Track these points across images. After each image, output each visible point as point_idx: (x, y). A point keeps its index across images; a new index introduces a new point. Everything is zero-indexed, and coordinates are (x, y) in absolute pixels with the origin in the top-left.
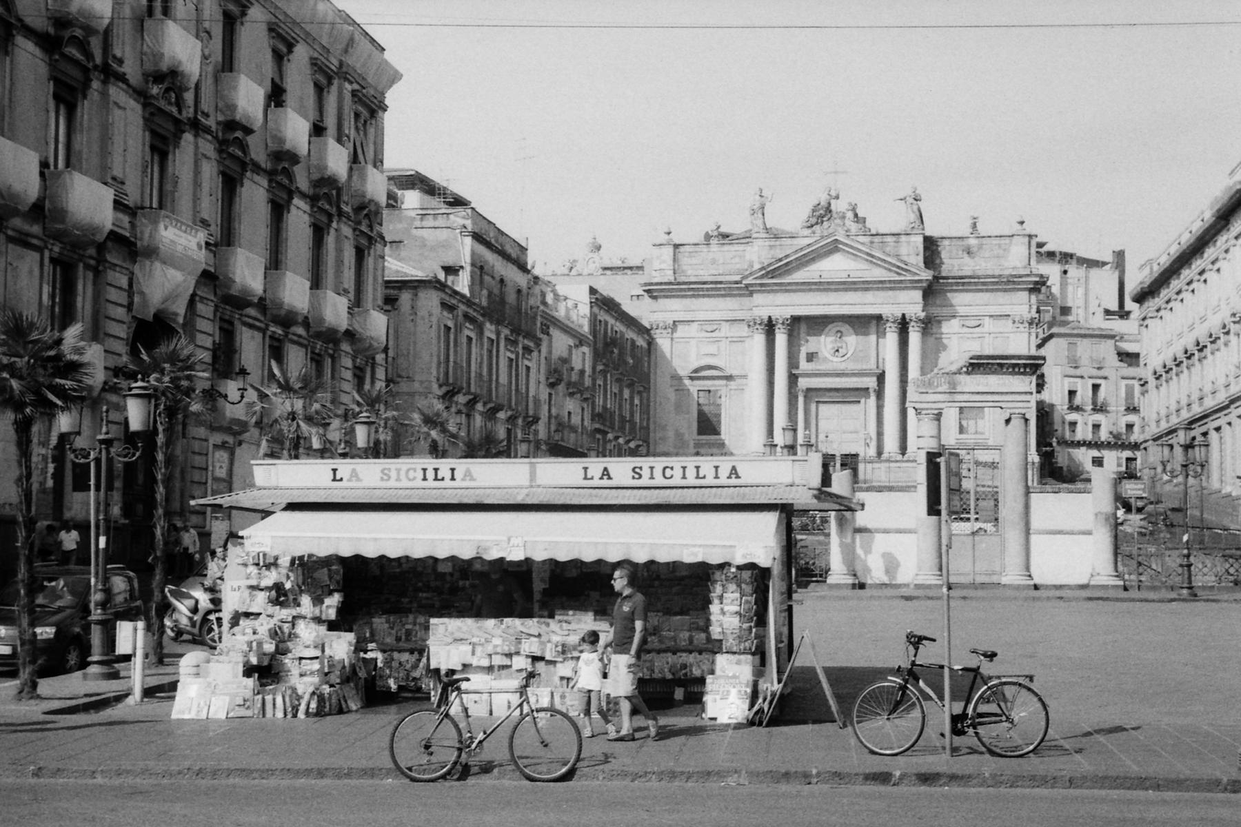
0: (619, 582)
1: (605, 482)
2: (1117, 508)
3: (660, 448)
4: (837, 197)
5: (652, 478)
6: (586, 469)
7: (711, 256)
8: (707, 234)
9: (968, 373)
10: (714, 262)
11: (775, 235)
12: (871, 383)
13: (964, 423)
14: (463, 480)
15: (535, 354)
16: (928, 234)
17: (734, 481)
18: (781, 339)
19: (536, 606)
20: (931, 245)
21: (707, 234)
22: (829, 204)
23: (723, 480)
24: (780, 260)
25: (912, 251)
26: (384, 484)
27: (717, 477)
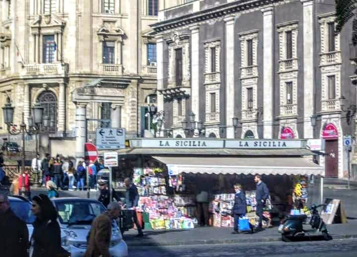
0: (257, 179)
1: (246, 147)
2: (21, 186)
5: (260, 146)
6: (161, 142)
9: (99, 87)
12: (62, 81)
14: (202, 146)
17: (284, 147)
19: (130, 247)
23: (281, 147)
26: (177, 147)
27: (279, 146)
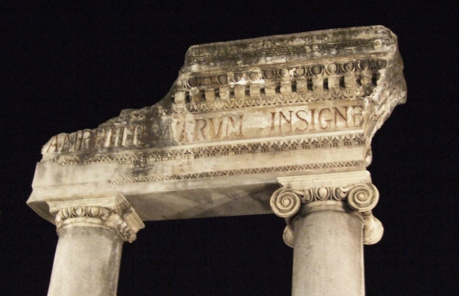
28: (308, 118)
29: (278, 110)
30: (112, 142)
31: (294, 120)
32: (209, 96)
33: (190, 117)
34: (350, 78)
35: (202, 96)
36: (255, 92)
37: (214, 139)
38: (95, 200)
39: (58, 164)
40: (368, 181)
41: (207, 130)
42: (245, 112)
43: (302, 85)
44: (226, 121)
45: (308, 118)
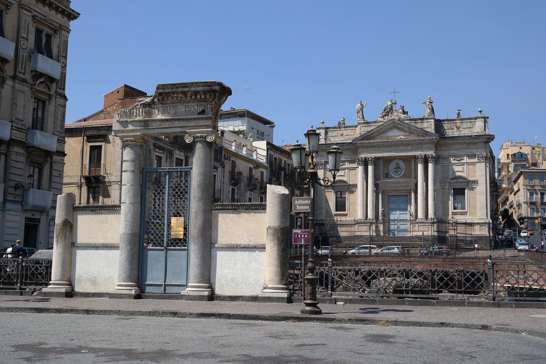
3: (50, 204)
4: (395, 104)
7: (341, 132)
8: (339, 122)
10: (342, 135)
11: (367, 123)
13: (456, 205)
15: (220, 169)
16: (437, 118)
18: (370, 168)
20: (439, 124)
21: (339, 122)
22: (392, 107)
24: (369, 132)
25: (429, 126)
28: (196, 108)
29: (187, 104)
30: (136, 114)
31: (192, 109)
32: (165, 99)
33: (160, 105)
34: (208, 96)
35: (163, 99)
36: (179, 98)
37: (54, 149)
38: (224, 346)
39: (64, 67)
40: (486, 166)
41: (166, 110)
42: (177, 105)
43: (193, 97)
44: (172, 108)
45: (196, 108)
